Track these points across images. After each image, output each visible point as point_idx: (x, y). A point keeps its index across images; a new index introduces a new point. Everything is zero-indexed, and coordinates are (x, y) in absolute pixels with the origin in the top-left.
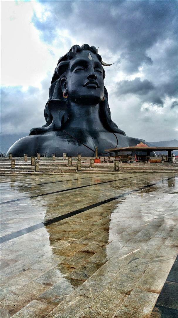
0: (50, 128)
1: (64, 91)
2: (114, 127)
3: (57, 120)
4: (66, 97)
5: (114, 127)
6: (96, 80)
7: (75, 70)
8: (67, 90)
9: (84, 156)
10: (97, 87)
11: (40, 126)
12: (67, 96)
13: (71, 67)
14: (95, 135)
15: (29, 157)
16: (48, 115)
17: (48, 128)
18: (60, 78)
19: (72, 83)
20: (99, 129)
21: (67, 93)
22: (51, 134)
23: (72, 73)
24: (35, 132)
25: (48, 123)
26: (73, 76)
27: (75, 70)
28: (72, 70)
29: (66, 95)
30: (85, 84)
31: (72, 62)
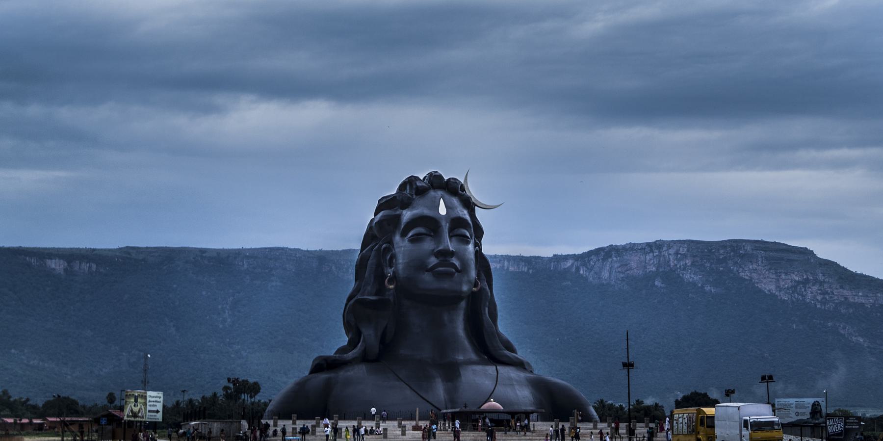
0: (356, 358)
1: (390, 272)
2: (501, 350)
3: (370, 334)
4: (391, 287)
5: (501, 350)
6: (453, 258)
7: (410, 234)
8: (394, 272)
9: (801, 398)
10: (454, 270)
11: (330, 352)
12: (395, 284)
13: (402, 226)
14: (451, 372)
15: (415, 430)
16: (352, 325)
17: (350, 355)
18: (381, 243)
19: (405, 261)
20: (462, 358)
21: (394, 278)
22: (359, 371)
23: (403, 241)
24: (323, 365)
25: (352, 344)
26: (405, 247)
27: (410, 234)
28: (404, 234)
29: (391, 281)
30: (430, 266)
31: (407, 215)
